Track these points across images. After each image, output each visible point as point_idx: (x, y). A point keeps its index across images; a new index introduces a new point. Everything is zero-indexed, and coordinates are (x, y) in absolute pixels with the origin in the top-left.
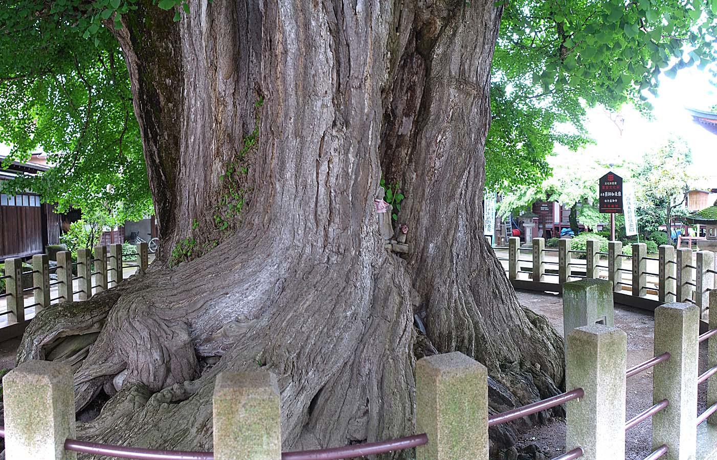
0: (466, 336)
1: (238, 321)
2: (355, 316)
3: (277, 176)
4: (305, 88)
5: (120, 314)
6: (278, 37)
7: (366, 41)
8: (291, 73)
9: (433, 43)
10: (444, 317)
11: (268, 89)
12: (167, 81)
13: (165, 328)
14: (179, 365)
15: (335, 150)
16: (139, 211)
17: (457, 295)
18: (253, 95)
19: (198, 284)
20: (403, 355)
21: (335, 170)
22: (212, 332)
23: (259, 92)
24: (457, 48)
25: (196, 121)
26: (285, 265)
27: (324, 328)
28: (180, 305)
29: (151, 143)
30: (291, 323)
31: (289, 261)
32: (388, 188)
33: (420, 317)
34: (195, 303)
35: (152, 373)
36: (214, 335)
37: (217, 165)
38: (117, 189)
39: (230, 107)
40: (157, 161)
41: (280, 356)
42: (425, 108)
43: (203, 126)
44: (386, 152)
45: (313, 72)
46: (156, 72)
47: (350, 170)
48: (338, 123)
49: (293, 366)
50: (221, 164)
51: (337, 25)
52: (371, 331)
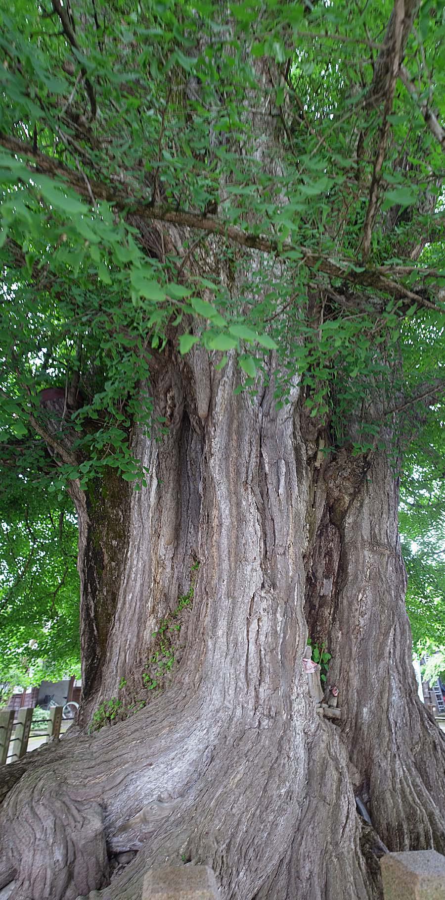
0: (422, 833)
1: (160, 800)
2: (290, 794)
3: (210, 633)
4: (236, 555)
5: (21, 796)
6: (215, 512)
7: (288, 516)
8: (225, 542)
9: (344, 514)
10: (390, 802)
11: (204, 555)
12: (114, 542)
13: (75, 812)
14: (86, 867)
15: (264, 610)
16: (60, 670)
17: (402, 773)
18: (189, 561)
19: (120, 753)
20: (349, 852)
21: (265, 628)
22: (130, 816)
23: (195, 557)
24: (366, 516)
25: (135, 580)
26: (214, 729)
27: (256, 810)
28: (97, 781)
29: (89, 597)
30: (220, 803)
31: (219, 724)
32: (315, 648)
33: (362, 800)
34: (114, 777)
35: (48, 882)
36: (132, 820)
37: (151, 622)
38: (41, 644)
39: (168, 570)
40: (92, 615)
41: (207, 847)
42: (343, 570)
43: (142, 585)
44: (310, 612)
45: (244, 542)
46: (105, 533)
47: (278, 629)
48: (266, 585)
49: (223, 862)
50: (154, 621)
51: (263, 504)
52: (309, 815)
